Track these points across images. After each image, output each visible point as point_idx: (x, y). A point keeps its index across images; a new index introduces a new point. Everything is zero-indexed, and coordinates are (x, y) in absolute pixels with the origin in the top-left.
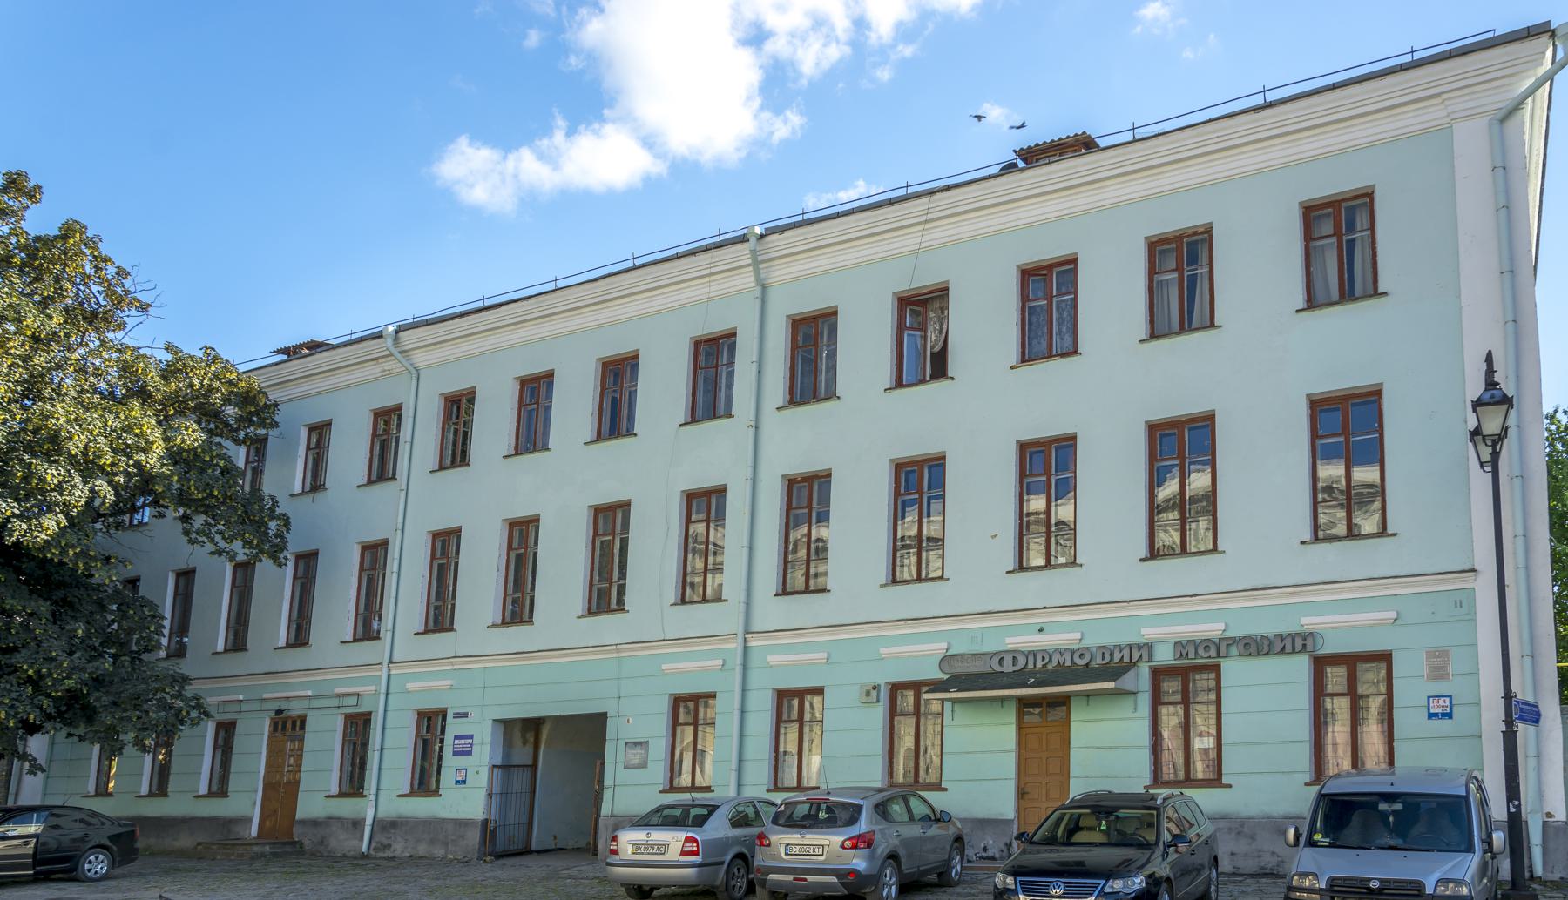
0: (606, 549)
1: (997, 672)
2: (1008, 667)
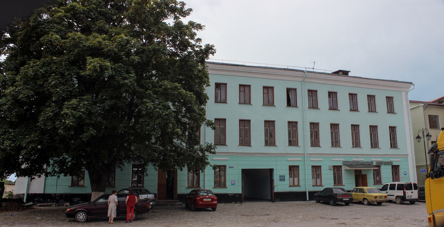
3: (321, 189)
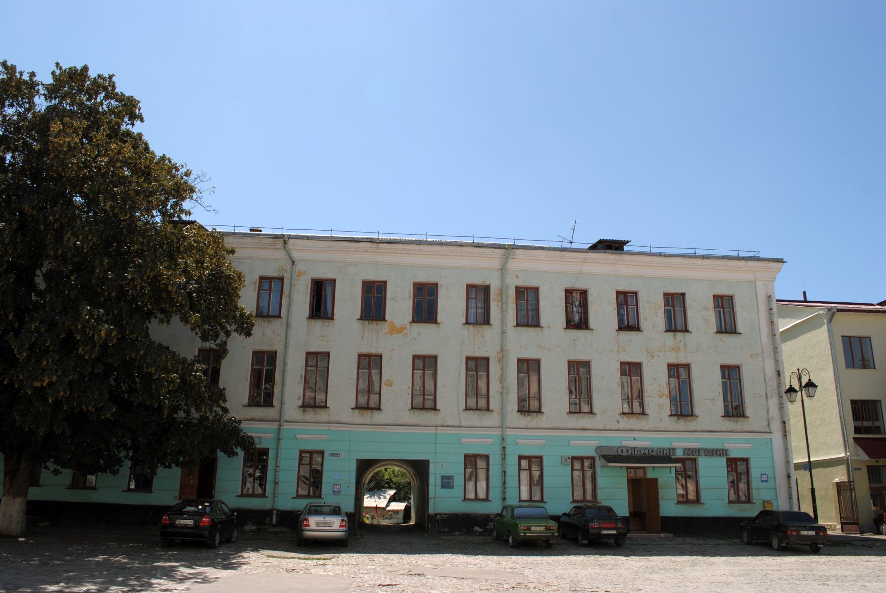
1: (620, 455)
2: (625, 454)
3: (751, 511)
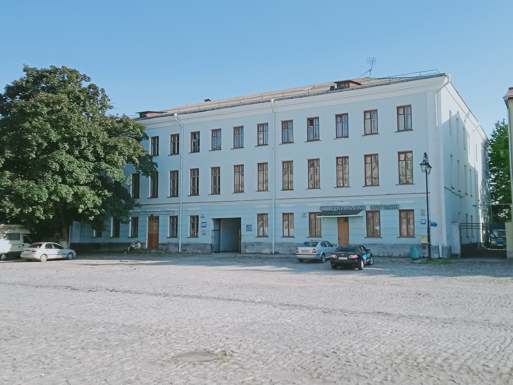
0: (194, 179)
